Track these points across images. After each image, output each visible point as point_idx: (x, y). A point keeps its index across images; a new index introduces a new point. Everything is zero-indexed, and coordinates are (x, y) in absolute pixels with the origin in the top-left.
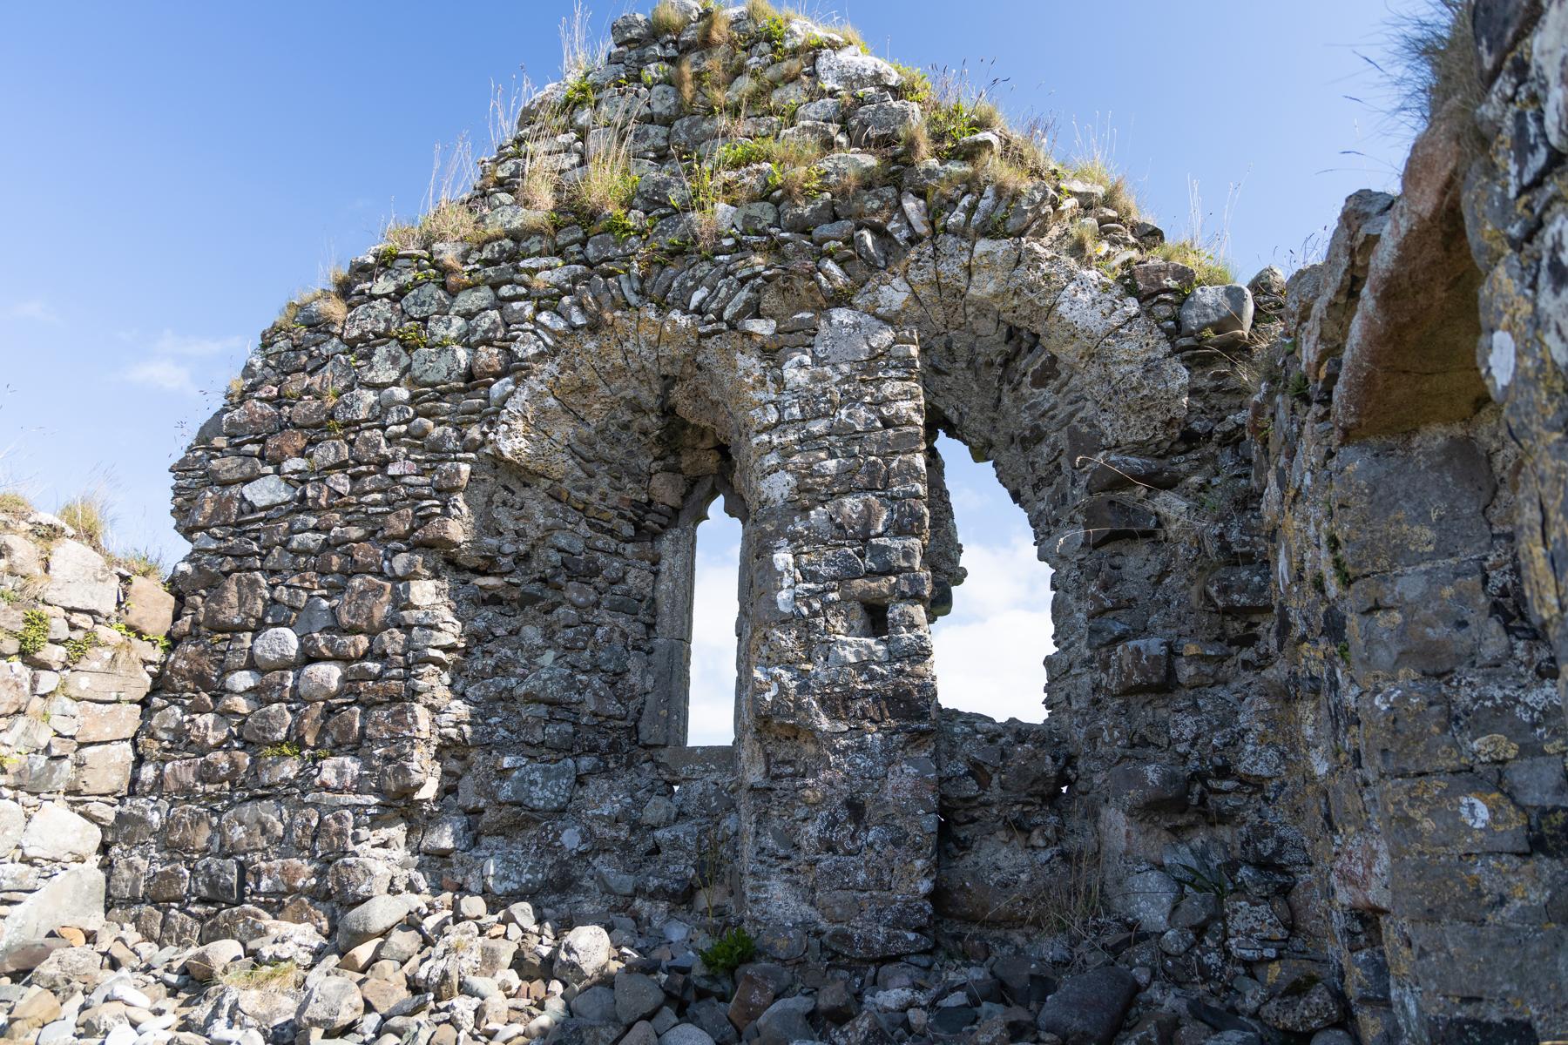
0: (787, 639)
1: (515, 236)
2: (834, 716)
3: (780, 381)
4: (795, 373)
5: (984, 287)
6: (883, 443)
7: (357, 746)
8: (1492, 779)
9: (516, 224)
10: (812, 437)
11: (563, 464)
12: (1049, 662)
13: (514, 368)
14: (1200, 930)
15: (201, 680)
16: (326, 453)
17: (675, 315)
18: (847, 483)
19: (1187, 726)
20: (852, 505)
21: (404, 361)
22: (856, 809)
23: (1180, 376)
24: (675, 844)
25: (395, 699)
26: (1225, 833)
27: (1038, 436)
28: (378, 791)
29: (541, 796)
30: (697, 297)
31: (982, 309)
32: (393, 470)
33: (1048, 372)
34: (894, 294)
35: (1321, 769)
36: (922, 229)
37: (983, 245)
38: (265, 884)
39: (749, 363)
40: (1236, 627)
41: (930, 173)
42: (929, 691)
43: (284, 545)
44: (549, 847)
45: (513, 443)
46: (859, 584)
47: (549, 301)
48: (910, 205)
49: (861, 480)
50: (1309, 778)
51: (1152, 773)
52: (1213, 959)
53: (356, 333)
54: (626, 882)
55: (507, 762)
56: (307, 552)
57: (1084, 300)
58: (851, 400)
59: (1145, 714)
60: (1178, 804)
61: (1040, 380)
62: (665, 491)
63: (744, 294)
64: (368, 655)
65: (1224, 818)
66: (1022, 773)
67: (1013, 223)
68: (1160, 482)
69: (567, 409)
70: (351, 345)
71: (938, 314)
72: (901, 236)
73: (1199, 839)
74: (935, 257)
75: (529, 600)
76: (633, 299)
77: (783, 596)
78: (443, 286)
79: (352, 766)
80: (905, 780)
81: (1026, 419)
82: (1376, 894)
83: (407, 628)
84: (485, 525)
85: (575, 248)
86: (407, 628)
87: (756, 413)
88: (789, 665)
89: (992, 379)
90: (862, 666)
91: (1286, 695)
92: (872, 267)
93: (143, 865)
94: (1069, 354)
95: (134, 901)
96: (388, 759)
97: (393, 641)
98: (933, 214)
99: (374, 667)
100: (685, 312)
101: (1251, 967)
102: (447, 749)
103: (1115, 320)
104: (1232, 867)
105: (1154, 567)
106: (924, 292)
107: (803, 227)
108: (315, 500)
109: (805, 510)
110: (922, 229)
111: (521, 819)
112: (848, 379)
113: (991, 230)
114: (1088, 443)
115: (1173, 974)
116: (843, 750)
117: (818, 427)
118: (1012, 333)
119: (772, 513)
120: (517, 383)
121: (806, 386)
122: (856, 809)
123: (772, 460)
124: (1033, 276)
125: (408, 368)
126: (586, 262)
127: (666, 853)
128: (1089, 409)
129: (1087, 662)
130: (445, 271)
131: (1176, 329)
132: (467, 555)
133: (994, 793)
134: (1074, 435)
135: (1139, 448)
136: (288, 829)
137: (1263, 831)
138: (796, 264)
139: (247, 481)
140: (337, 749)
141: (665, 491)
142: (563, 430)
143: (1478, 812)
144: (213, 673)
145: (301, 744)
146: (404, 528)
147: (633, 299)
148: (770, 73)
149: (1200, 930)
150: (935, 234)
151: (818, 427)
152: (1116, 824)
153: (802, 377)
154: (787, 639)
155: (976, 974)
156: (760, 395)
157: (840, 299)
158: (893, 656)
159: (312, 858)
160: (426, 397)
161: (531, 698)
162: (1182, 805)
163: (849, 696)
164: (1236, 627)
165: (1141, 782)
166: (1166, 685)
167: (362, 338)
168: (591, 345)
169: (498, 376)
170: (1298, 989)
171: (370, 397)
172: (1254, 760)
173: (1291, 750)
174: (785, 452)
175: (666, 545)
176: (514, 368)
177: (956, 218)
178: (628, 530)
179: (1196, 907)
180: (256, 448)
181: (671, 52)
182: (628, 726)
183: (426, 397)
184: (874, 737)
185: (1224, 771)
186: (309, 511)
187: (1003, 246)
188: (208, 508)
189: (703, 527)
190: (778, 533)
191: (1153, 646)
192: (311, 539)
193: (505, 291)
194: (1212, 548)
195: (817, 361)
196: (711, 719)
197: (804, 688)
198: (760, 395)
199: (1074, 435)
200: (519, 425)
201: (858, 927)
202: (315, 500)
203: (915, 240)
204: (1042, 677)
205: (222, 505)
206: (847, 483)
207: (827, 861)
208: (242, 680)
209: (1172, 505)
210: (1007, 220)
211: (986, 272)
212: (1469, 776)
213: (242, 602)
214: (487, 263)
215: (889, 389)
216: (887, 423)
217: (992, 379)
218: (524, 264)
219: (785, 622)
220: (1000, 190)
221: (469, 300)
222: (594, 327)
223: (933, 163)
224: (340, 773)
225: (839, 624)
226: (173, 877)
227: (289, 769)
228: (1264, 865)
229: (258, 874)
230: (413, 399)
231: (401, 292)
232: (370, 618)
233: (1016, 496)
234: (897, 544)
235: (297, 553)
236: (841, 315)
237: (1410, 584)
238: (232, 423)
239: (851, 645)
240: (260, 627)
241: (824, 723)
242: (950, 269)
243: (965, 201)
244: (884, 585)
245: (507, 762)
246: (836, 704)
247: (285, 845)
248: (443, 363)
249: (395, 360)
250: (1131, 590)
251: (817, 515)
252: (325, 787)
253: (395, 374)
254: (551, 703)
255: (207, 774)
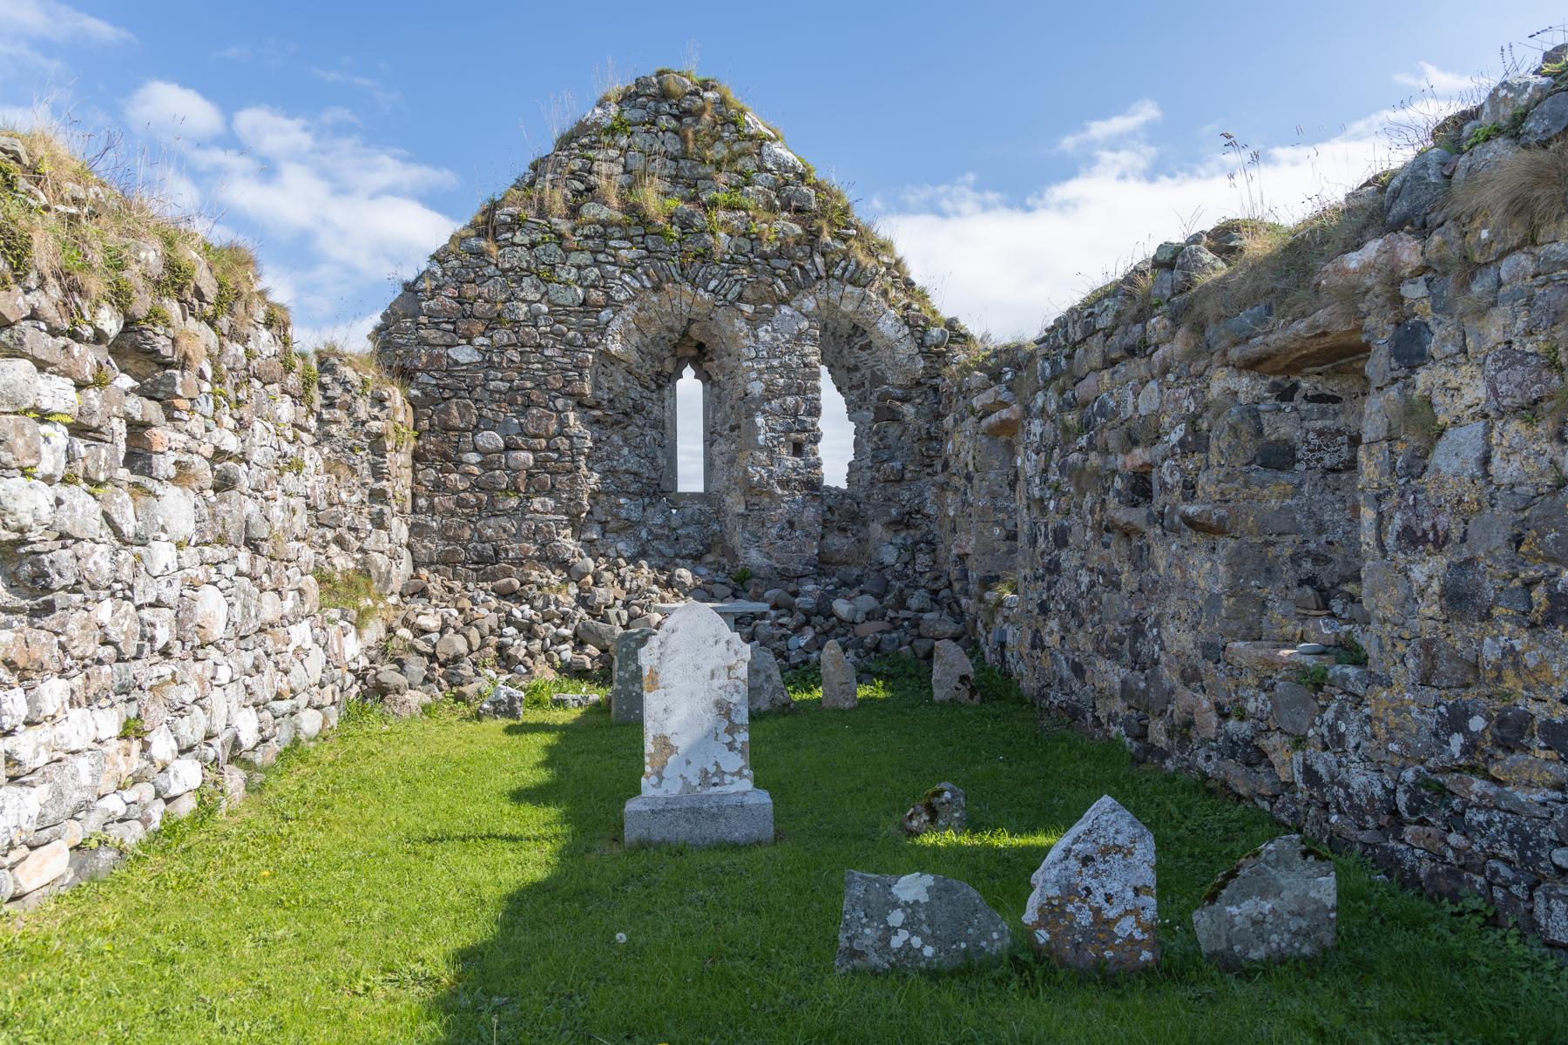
0: (763, 456)
1: (604, 224)
2: (783, 488)
3: (756, 337)
4: (764, 334)
5: (848, 307)
6: (804, 375)
7: (551, 492)
8: (1001, 524)
9: (603, 216)
10: (772, 367)
11: (635, 356)
12: (850, 465)
13: (610, 302)
14: (906, 564)
15: (446, 457)
16: (501, 336)
17: (701, 291)
18: (787, 390)
19: (907, 495)
20: (790, 400)
21: (543, 289)
22: (791, 524)
23: (921, 363)
24: (688, 536)
25: (570, 472)
26: (912, 532)
27: (856, 368)
28: (566, 514)
29: (635, 516)
30: (712, 284)
31: (844, 315)
32: (548, 352)
33: (868, 346)
34: (809, 304)
35: (952, 513)
36: (823, 274)
37: (849, 288)
38: (511, 554)
39: (740, 324)
40: (927, 461)
41: (827, 245)
42: (820, 480)
43: (483, 386)
44: (638, 538)
45: (615, 347)
46: (793, 435)
47: (630, 268)
48: (818, 260)
49: (794, 390)
50: (946, 515)
51: (894, 512)
52: (910, 572)
53: (507, 266)
54: (670, 552)
55: (622, 501)
56: (500, 392)
57: (888, 325)
58: (791, 352)
59: (891, 490)
60: (900, 522)
61: (862, 348)
62: (669, 366)
63: (737, 288)
64: (548, 448)
65: (916, 527)
66: (847, 510)
67: (863, 281)
68: (904, 400)
69: (638, 328)
70: (504, 272)
71: (825, 313)
72: (813, 275)
73: (903, 534)
74: (828, 288)
75: (618, 422)
76: (678, 278)
77: (761, 438)
78: (560, 245)
79: (551, 503)
80: (810, 513)
81: (853, 361)
82: (968, 550)
83: (569, 437)
84: (597, 386)
85: (640, 239)
86: (569, 437)
87: (745, 350)
88: (763, 467)
89: (846, 345)
90: (794, 469)
91: (944, 487)
92: (799, 286)
93: (433, 547)
94: (877, 343)
95: (432, 563)
96: (570, 499)
97: (563, 444)
98: (829, 266)
99: (555, 456)
100: (706, 290)
101: (921, 574)
102: (594, 495)
103: (900, 335)
104: (916, 543)
105: (898, 432)
106: (822, 304)
107: (765, 257)
108: (500, 363)
109: (769, 400)
110: (823, 274)
111: (628, 526)
112: (788, 342)
113: (853, 283)
114: (878, 380)
115: (900, 576)
116: (787, 502)
117: (775, 363)
118: (855, 327)
119: (754, 399)
120: (615, 313)
121: (763, 342)
122: (791, 524)
123: (754, 375)
124: (869, 308)
125: (547, 293)
126: (646, 248)
127: (682, 540)
128: (883, 366)
129: (869, 468)
130: (560, 236)
131: (921, 345)
132: (589, 400)
133: (836, 517)
134: (873, 373)
135: (900, 387)
136: (519, 529)
137: (929, 532)
138: (764, 278)
139: (448, 346)
140: (537, 493)
141: (669, 366)
142: (635, 339)
143: (997, 531)
144: (452, 453)
145: (517, 490)
146: (559, 385)
147: (678, 278)
148: (736, 147)
149: (906, 564)
150: (828, 277)
151: (775, 363)
152: (877, 529)
153: (768, 338)
154: (763, 456)
155: (835, 580)
156: (746, 342)
157: (785, 301)
158: (807, 466)
159: (535, 542)
160: (558, 312)
161: (627, 472)
162: (902, 522)
163: (789, 481)
164: (927, 461)
165: (889, 514)
166: (900, 479)
167: (512, 269)
168: (655, 299)
169: (604, 307)
170: (936, 579)
171: (524, 308)
172: (930, 509)
173: (942, 505)
174: (760, 372)
175: (666, 392)
176: (617, 307)
177: (838, 272)
178: (654, 387)
179: (906, 556)
180: (451, 327)
181: (675, 112)
182: (656, 485)
183: (558, 312)
184: (799, 497)
185: (918, 512)
186: (497, 369)
187: (858, 291)
188: (424, 359)
189: (679, 382)
190: (757, 409)
191: (897, 465)
192: (504, 386)
193: (601, 257)
194: (924, 432)
195: (774, 330)
196: (690, 475)
197: (770, 476)
198: (746, 342)
199: (873, 373)
200: (618, 337)
201: (792, 566)
202: (500, 363)
203: (819, 278)
204: (846, 469)
205: (433, 359)
206: (787, 390)
207: (780, 543)
208: (474, 458)
209: (908, 410)
210: (859, 279)
211: (848, 301)
212: (997, 523)
213: (462, 417)
214: (587, 237)
215: (807, 349)
216: (806, 365)
217: (846, 345)
218: (612, 243)
219: (761, 449)
220: (858, 264)
221: (577, 258)
222: (657, 289)
223: (829, 239)
224: (544, 505)
225: (784, 451)
226: (455, 552)
227: (514, 502)
228: (929, 543)
229: (506, 551)
230: (551, 313)
231: (533, 245)
232: (547, 430)
233: (839, 389)
234: (809, 419)
235: (492, 392)
236: (785, 310)
237: (992, 476)
238: (429, 309)
239: (790, 461)
240: (476, 429)
241: (779, 491)
242: (834, 296)
243: (843, 264)
244: (803, 436)
245: (622, 501)
246: (784, 484)
247: (517, 537)
248: (569, 295)
249: (537, 288)
250: (890, 441)
251: (775, 403)
252: (536, 511)
253: (538, 296)
254: (635, 474)
255: (461, 503)
